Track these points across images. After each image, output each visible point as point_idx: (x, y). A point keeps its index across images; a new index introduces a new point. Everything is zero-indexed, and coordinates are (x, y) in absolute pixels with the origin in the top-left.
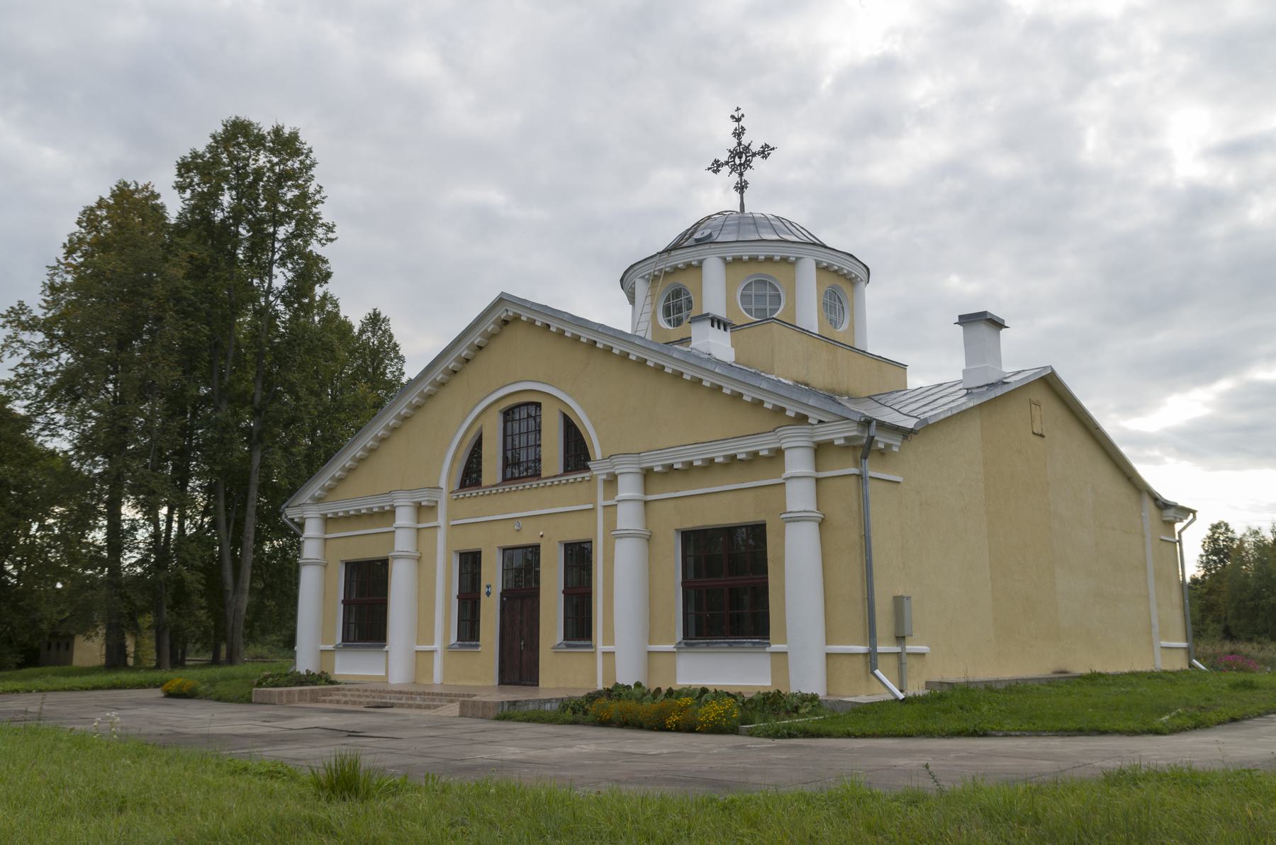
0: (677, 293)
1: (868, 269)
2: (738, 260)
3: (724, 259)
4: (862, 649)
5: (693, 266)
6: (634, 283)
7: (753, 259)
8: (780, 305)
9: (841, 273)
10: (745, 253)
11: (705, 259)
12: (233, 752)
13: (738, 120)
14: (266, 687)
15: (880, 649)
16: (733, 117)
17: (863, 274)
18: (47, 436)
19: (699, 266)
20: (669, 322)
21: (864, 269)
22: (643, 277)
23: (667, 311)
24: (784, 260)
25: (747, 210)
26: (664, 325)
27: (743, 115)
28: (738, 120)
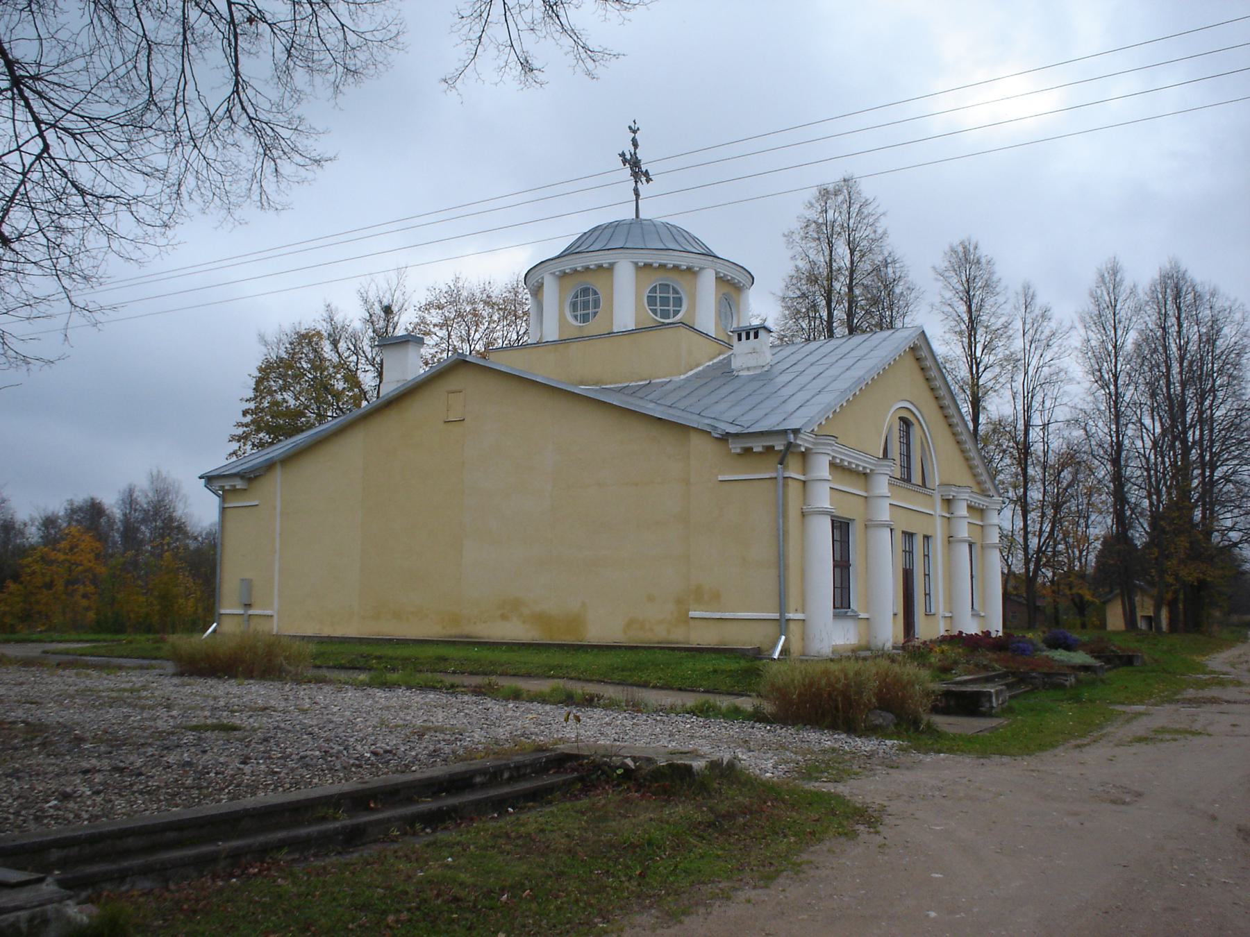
0: (585, 291)
1: (753, 279)
2: (648, 266)
3: (636, 264)
4: (776, 616)
5: (604, 268)
6: (543, 278)
7: (662, 267)
8: (681, 306)
9: (725, 279)
10: (656, 259)
11: (615, 263)
12: (277, 557)
13: (635, 132)
14: (389, 820)
15: (791, 616)
16: (630, 128)
17: (747, 281)
18: (41, 632)
19: (611, 267)
20: (576, 317)
21: (748, 276)
22: (553, 274)
23: (574, 306)
24: (689, 269)
25: (642, 216)
26: (570, 319)
27: (638, 129)
28: (635, 132)
